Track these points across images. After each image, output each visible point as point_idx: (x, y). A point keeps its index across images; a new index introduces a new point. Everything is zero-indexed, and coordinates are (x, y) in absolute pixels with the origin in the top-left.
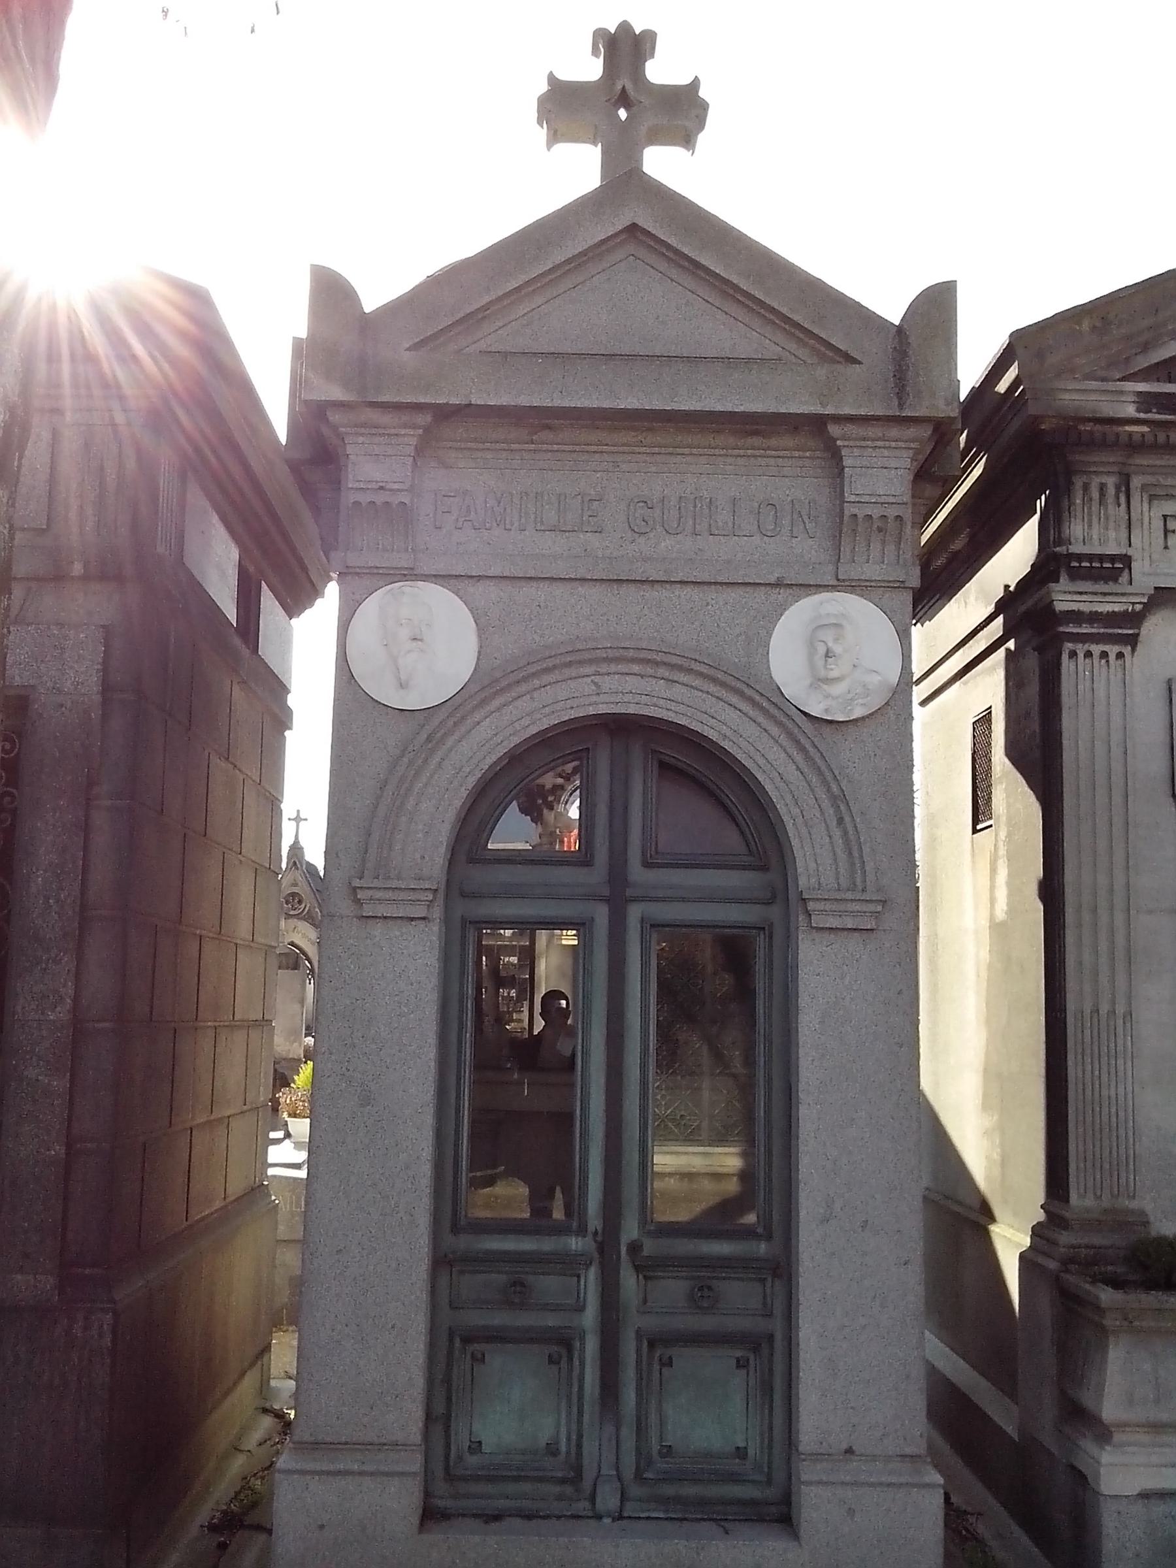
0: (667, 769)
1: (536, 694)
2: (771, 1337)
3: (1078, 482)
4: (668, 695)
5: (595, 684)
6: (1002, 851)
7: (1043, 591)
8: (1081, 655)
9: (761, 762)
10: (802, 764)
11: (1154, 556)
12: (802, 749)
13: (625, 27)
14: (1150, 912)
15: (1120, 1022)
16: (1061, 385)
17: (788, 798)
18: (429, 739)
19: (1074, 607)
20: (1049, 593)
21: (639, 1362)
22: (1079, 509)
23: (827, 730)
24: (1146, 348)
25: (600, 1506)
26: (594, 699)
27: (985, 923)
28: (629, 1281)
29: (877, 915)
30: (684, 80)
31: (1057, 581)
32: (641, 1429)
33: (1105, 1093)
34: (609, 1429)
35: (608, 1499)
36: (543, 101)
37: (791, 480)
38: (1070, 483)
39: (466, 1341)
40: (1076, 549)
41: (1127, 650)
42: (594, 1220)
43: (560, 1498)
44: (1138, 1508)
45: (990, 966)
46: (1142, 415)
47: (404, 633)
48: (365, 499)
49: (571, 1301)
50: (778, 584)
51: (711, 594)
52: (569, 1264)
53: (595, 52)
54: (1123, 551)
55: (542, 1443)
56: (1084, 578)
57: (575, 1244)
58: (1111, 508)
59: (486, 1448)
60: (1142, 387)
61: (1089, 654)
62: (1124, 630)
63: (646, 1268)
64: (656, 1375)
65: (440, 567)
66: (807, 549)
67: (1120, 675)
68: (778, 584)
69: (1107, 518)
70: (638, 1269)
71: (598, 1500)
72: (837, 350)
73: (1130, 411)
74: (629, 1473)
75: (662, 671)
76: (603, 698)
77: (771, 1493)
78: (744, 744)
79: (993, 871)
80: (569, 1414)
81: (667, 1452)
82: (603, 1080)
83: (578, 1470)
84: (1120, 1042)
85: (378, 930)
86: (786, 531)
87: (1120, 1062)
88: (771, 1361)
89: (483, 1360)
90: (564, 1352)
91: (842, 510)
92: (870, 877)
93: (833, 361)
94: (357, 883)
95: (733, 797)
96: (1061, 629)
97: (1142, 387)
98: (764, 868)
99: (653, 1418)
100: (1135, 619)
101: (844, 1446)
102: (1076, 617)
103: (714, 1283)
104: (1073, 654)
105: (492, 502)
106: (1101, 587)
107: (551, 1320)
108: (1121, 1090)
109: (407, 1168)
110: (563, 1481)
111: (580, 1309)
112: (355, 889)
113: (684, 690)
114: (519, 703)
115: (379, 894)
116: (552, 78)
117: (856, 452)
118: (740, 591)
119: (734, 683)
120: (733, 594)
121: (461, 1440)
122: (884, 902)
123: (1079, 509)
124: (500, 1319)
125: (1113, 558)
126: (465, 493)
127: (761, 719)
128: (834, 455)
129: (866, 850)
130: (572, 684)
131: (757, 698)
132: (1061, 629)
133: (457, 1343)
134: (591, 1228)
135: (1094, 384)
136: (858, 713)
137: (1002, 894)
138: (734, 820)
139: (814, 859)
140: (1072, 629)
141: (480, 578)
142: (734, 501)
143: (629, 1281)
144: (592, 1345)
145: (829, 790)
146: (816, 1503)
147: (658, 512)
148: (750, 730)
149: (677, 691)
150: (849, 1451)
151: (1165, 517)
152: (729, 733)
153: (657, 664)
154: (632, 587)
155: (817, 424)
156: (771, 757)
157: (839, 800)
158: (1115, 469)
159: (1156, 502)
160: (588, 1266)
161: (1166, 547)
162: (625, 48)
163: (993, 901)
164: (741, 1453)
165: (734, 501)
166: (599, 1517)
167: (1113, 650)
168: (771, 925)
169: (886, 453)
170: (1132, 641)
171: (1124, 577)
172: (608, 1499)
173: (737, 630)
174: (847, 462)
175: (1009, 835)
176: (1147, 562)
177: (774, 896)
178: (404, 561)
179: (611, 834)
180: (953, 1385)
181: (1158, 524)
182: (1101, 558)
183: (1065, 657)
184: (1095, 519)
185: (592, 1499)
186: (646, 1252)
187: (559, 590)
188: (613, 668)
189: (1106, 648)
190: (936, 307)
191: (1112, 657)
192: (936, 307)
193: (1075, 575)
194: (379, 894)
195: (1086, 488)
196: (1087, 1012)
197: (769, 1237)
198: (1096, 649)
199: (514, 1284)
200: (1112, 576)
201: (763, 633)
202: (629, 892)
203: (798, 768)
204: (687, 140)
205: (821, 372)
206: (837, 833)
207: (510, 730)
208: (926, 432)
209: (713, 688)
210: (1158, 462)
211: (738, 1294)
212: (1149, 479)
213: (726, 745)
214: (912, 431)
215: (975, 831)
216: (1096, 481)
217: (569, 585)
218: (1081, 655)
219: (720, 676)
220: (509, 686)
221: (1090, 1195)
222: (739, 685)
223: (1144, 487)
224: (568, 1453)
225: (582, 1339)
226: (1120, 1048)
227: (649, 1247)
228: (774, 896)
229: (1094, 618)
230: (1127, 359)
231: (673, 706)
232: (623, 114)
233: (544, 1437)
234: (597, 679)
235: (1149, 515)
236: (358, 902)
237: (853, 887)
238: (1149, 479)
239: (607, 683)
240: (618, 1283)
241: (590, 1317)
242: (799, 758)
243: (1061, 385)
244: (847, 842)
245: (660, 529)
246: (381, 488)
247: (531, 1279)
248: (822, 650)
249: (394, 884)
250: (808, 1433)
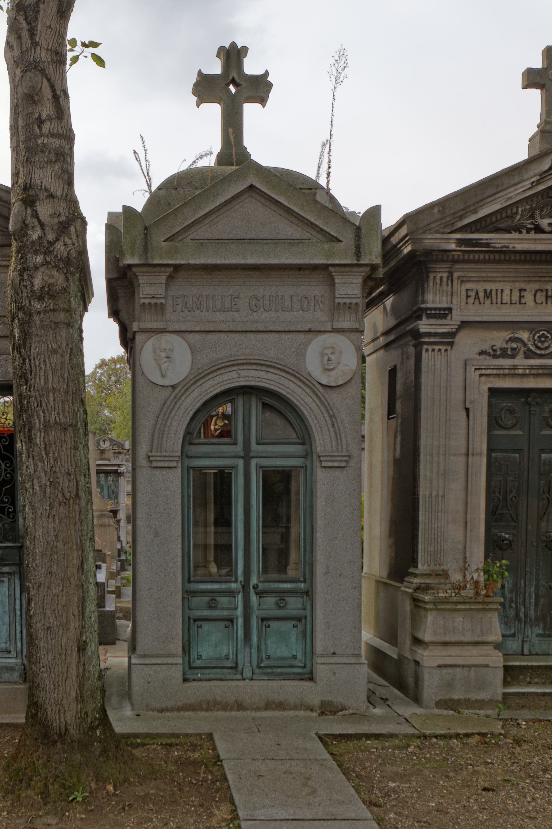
0: (265, 406)
1: (215, 379)
2: (306, 617)
3: (431, 276)
4: (266, 377)
5: (238, 374)
6: (399, 429)
7: (416, 324)
8: (430, 350)
9: (303, 402)
10: (318, 403)
11: (462, 307)
12: (318, 397)
13: (233, 45)
14: (454, 455)
15: (440, 499)
16: (424, 236)
17: (313, 417)
18: (175, 398)
19: (428, 330)
20: (418, 325)
21: (258, 628)
22: (431, 288)
23: (328, 390)
24: (461, 218)
25: (245, 676)
26: (238, 380)
27: (391, 459)
28: (254, 598)
29: (347, 462)
30: (261, 72)
31: (421, 320)
32: (259, 649)
33: (433, 526)
34: (247, 650)
35: (247, 673)
36: (196, 85)
37: (315, 289)
38: (428, 277)
39: (195, 620)
40: (430, 305)
41: (449, 348)
42: (241, 578)
43: (230, 674)
44: (437, 671)
45: (394, 478)
46: (458, 248)
47: (163, 355)
48: (147, 301)
49: (233, 606)
50: (310, 331)
51: (283, 335)
52: (231, 593)
53: (218, 56)
54: (448, 306)
55: (223, 655)
56: (432, 318)
57: (233, 586)
58: (445, 288)
59: (203, 657)
60: (458, 236)
61: (433, 350)
62: (448, 339)
63: (260, 594)
64: (264, 631)
65: (176, 327)
66: (320, 316)
67: (446, 358)
68: (310, 331)
69: (443, 291)
70: (257, 594)
71: (244, 673)
72: (333, 236)
73: (453, 246)
74: (255, 663)
75: (264, 368)
76: (241, 379)
77: (307, 670)
78: (296, 396)
79: (395, 437)
80: (233, 646)
81: (268, 657)
82: (242, 526)
83: (237, 663)
84: (440, 507)
85: (158, 472)
86: (312, 308)
87: (440, 514)
88: (306, 625)
89: (201, 627)
90: (230, 624)
91: (334, 300)
92: (344, 447)
93: (333, 241)
94: (150, 454)
95: (282, 408)
96: (422, 340)
97: (458, 236)
98: (303, 444)
99: (263, 647)
100: (452, 335)
101: (332, 652)
102: (429, 334)
103: (286, 598)
104: (427, 350)
105: (195, 300)
106: (440, 322)
107: (226, 613)
108: (439, 525)
109: (173, 559)
110: (231, 668)
111: (236, 609)
112: (149, 457)
113: (273, 375)
114: (209, 382)
115: (159, 458)
116: (200, 73)
117: (340, 277)
118: (294, 334)
119: (292, 372)
120: (292, 336)
121: (194, 655)
122: (349, 456)
123: (431, 288)
124: (206, 613)
125: (444, 309)
126: (185, 296)
127: (302, 386)
128: (332, 278)
129: (343, 436)
130: (229, 374)
131: (302, 378)
132: (422, 340)
133: (192, 621)
134: (239, 580)
135: (438, 236)
136: (340, 382)
137: (398, 447)
138: (294, 428)
139: (322, 441)
140: (426, 340)
141: (191, 332)
142: (291, 297)
143: (254, 598)
144: (240, 621)
145: (329, 413)
146: (322, 671)
147: (261, 301)
148: (298, 391)
149: (270, 376)
150: (334, 653)
151: (467, 290)
152: (290, 392)
153: (262, 365)
154: (251, 334)
155: (326, 267)
156: (306, 401)
157: (332, 417)
158: (447, 270)
159: (463, 284)
160: (239, 593)
161: (467, 303)
162: (233, 55)
163: (395, 449)
164: (295, 657)
165: (291, 297)
166: (244, 679)
167: (443, 348)
168: (306, 466)
169: (352, 277)
170: (451, 344)
171: (449, 317)
172: (247, 673)
173: (293, 350)
174: (337, 281)
175: (402, 423)
176: (459, 310)
177: (307, 455)
178: (161, 325)
179: (244, 431)
180: (374, 647)
181: (464, 293)
182: (440, 309)
183: (424, 351)
184: (438, 293)
185: (242, 673)
186: (259, 588)
187: (222, 336)
188: (245, 367)
189: (441, 347)
190: (375, 212)
191: (443, 351)
192: (375, 212)
193: (429, 316)
194: (159, 458)
195: (435, 278)
196: (427, 496)
197: (305, 581)
198: (437, 348)
199: (212, 600)
200: (444, 316)
201: (303, 351)
202: (251, 454)
203: (317, 405)
204: (263, 101)
205: (326, 246)
206: (332, 430)
207: (205, 393)
208: (368, 269)
209: (284, 374)
210: (465, 267)
211: (294, 604)
212: (461, 274)
213: (289, 396)
214: (362, 269)
215: (389, 419)
216: (439, 275)
217: (227, 334)
218: (430, 350)
219: (287, 369)
220: (205, 376)
221: (426, 565)
222: (294, 373)
223: (459, 277)
224: (233, 658)
225: (237, 619)
226: (440, 508)
227: (261, 586)
228: (307, 455)
229: (436, 335)
230: (453, 223)
231: (268, 381)
232: (232, 88)
233: (225, 652)
234: (239, 372)
235: (461, 289)
236: (151, 462)
237: (337, 451)
238: (461, 274)
239: (244, 373)
240: (249, 599)
241: (240, 611)
242: (317, 401)
243: (424, 236)
244: (335, 433)
245: (262, 309)
246: (153, 297)
247: (218, 598)
248: (326, 358)
249: (164, 454)
250: (319, 648)
